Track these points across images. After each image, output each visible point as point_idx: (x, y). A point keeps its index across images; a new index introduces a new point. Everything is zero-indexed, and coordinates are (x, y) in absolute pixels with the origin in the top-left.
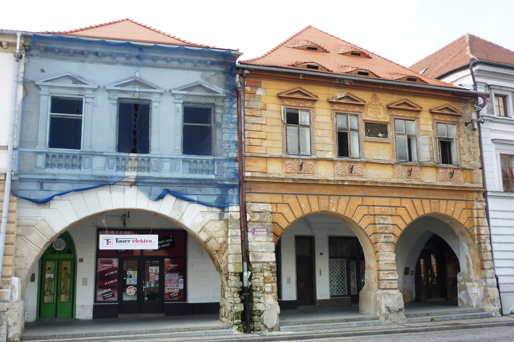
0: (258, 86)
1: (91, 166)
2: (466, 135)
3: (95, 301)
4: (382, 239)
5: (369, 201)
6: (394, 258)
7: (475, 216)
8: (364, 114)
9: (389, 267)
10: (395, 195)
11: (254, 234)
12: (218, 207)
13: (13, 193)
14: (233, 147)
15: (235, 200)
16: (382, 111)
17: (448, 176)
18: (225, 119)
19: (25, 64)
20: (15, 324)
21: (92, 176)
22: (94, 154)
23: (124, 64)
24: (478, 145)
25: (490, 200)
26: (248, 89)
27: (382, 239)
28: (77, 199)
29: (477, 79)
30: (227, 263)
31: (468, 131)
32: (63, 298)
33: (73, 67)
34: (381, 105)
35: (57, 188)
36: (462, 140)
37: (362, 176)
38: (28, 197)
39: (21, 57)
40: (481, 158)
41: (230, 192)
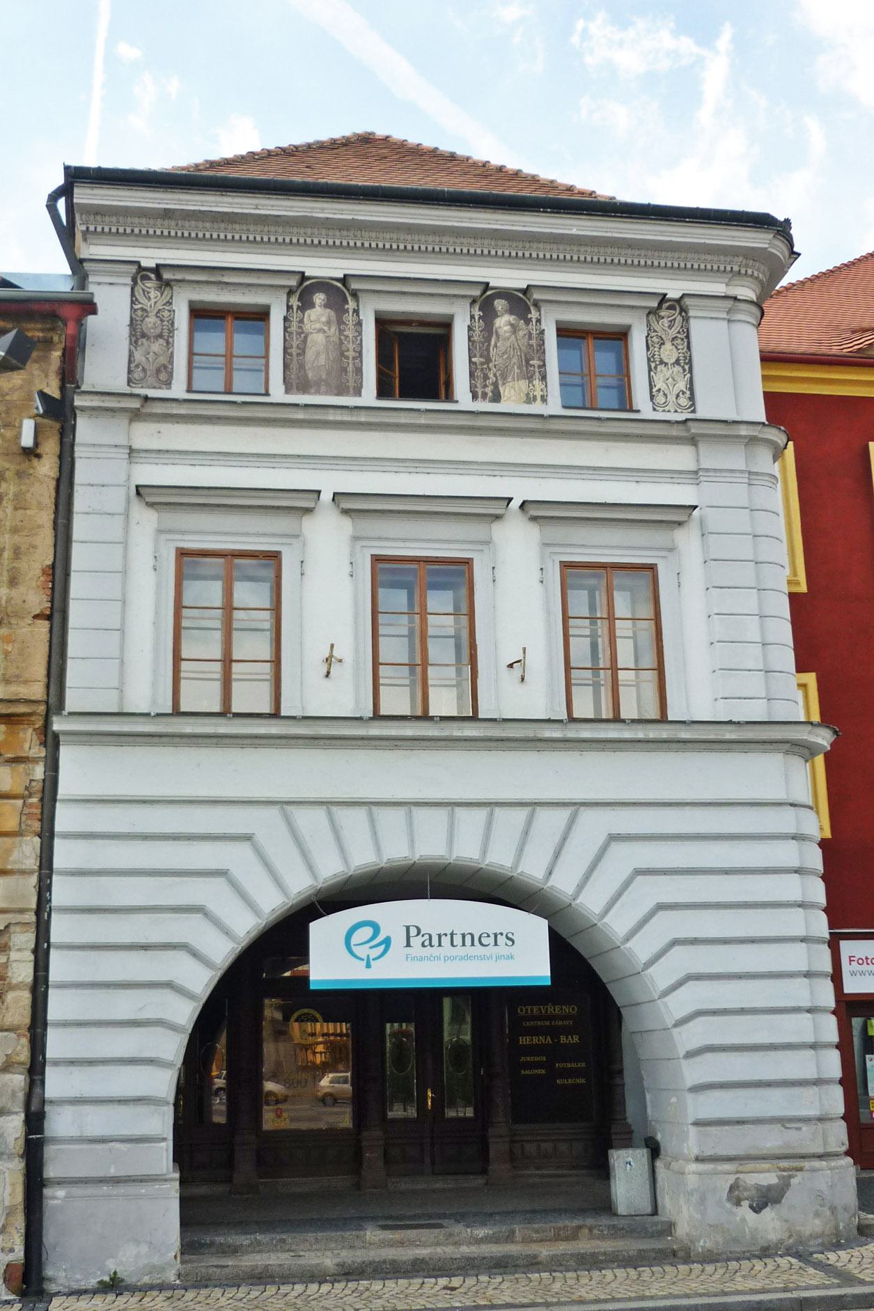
24: (45, 518)
40: (58, 576)
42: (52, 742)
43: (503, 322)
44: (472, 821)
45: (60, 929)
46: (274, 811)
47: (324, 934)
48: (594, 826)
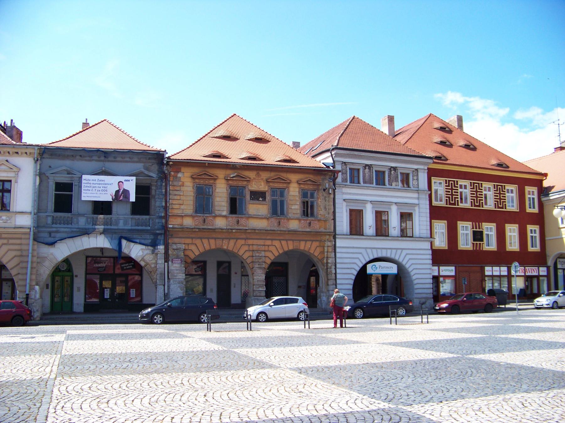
0: (178, 171)
1: (78, 223)
2: (323, 197)
3: (85, 301)
4: (257, 266)
5: (250, 242)
6: (264, 277)
7: (326, 250)
8: (249, 186)
9: (260, 283)
10: (268, 237)
11: (172, 262)
12: (151, 246)
13: (35, 239)
14: (162, 210)
15: (162, 242)
16: (262, 184)
17: (307, 225)
18: (157, 192)
19: (40, 165)
20: (37, 311)
21: (78, 228)
22: (79, 215)
23: (97, 161)
24: (332, 204)
25: (337, 240)
26: (172, 173)
27: (257, 266)
28: (70, 242)
29: (336, 159)
30: (157, 279)
31: (325, 195)
32: (66, 299)
33: (68, 163)
34: (262, 179)
35: (59, 235)
36: (320, 200)
37: (246, 226)
38: (42, 241)
39: (38, 160)
40: (334, 213)
41: (159, 237)
42: (335, 238)
43: (393, 172)
44: (389, 251)
45: (338, 266)
46: (364, 250)
47: (369, 266)
48: (404, 252)
